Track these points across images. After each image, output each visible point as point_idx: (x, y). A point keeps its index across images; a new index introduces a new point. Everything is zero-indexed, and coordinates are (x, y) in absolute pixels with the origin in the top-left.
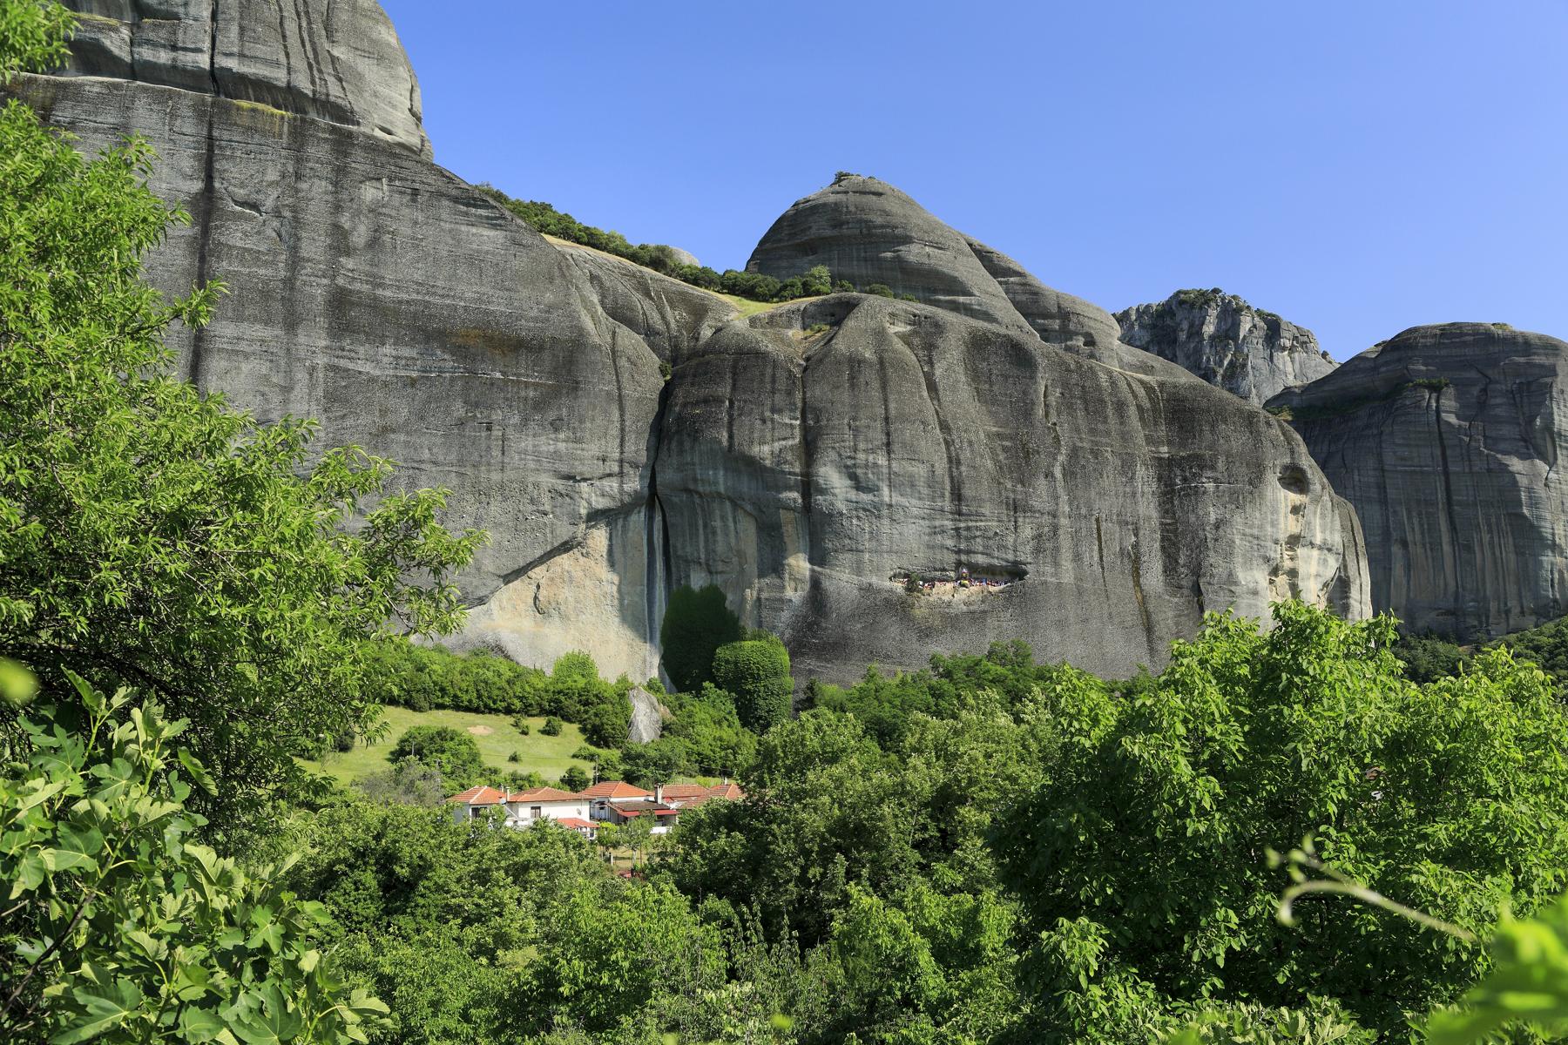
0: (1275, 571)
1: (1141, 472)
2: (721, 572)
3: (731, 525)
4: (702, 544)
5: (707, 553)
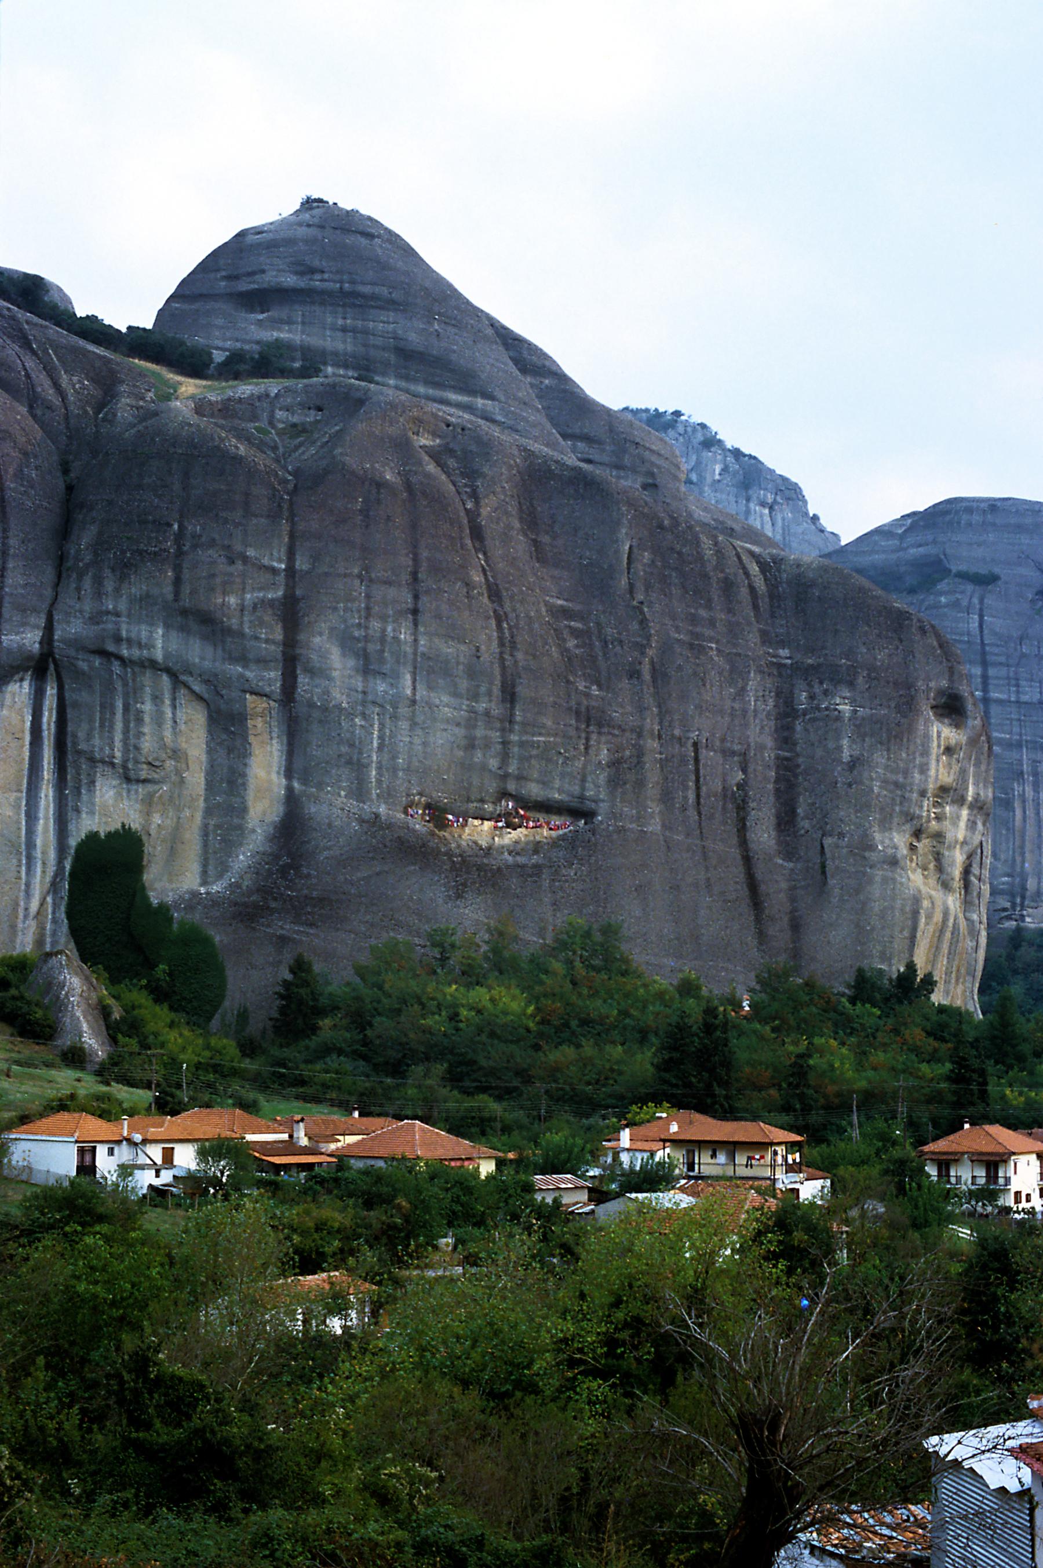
0: (917, 834)
1: (754, 682)
2: (145, 781)
3: (168, 713)
4: (118, 737)
5: (126, 750)
